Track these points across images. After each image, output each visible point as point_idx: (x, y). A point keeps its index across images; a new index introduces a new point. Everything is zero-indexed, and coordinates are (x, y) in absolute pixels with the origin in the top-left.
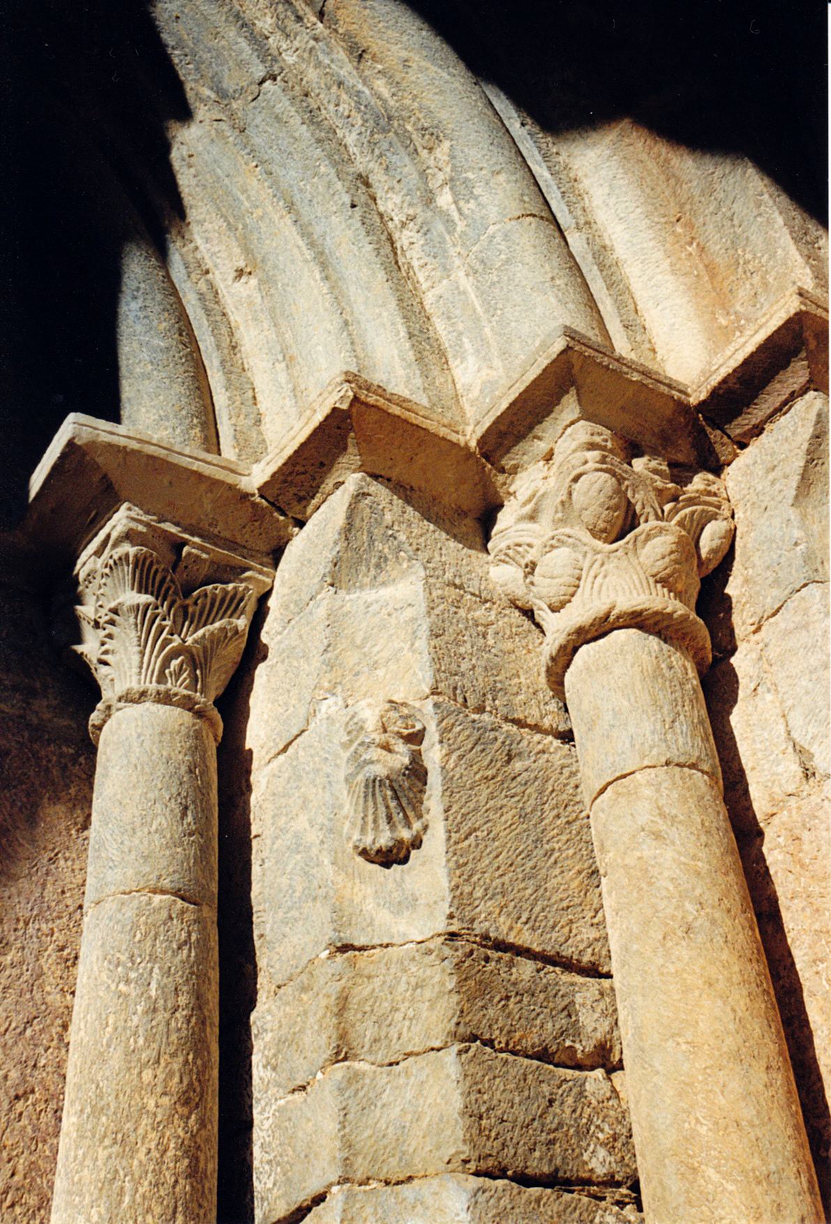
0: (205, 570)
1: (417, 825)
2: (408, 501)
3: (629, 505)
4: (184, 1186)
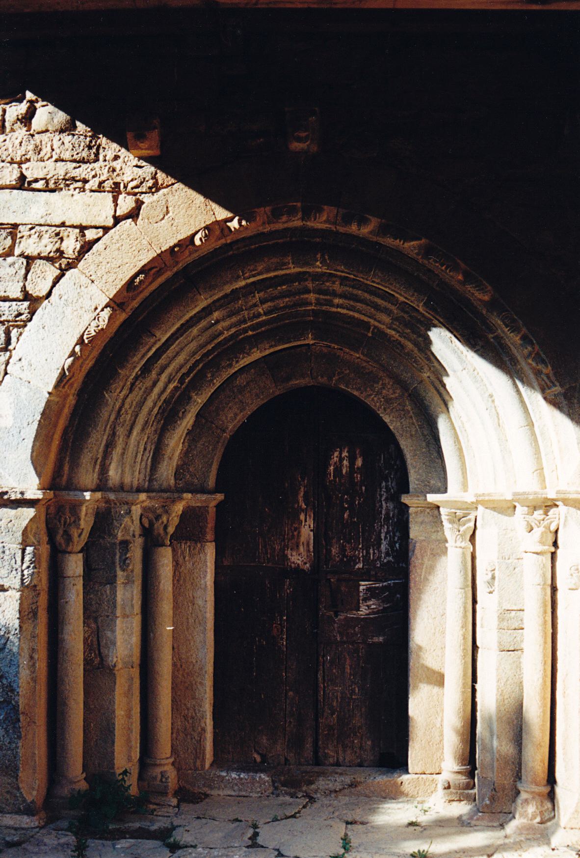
0: (462, 516)
1: (493, 588)
2: (495, 511)
3: (531, 526)
4: (462, 641)
